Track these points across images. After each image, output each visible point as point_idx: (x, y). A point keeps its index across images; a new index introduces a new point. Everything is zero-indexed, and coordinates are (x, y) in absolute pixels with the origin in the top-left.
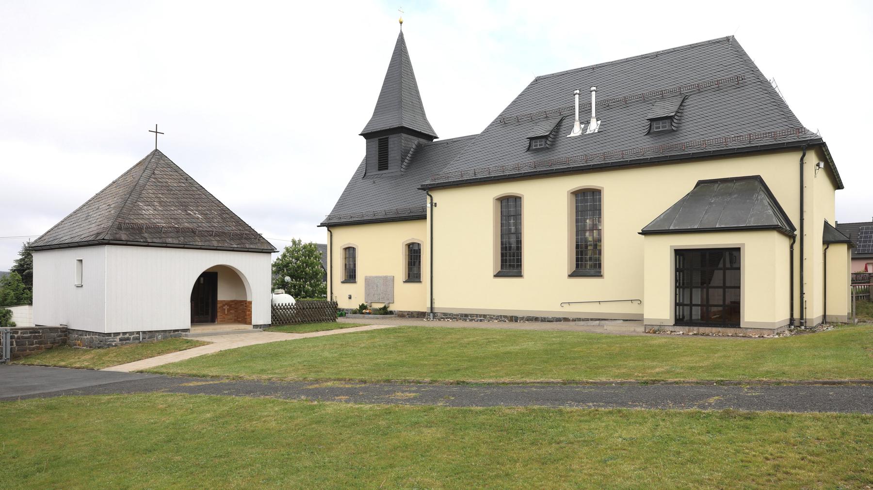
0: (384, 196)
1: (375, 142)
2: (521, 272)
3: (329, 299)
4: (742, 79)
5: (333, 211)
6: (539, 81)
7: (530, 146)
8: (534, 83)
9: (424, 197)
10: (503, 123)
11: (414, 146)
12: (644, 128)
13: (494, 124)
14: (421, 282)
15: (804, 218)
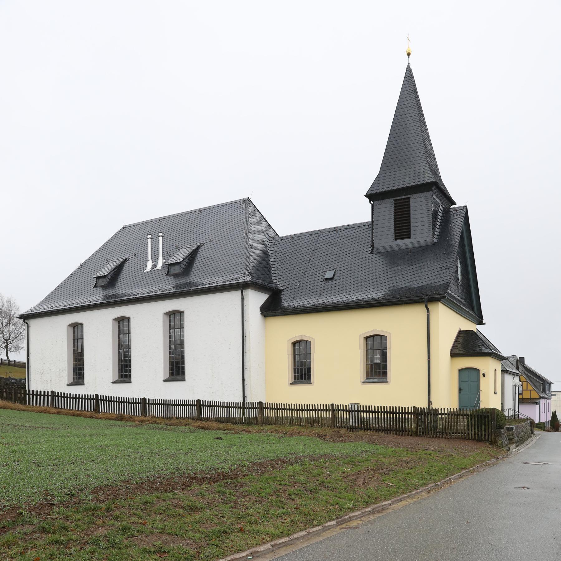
1: (388, 206)
2: (184, 378)
14: (387, 382)
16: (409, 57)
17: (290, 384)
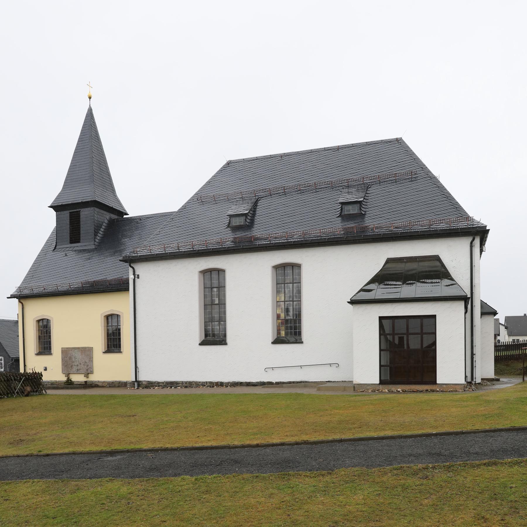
0: (78, 269)
2: (301, 339)
3: (22, 371)
4: (415, 174)
5: (23, 283)
6: (231, 165)
7: (229, 223)
8: (226, 166)
9: (127, 269)
10: (200, 201)
11: (106, 221)
12: (335, 211)
13: (190, 201)
14: (121, 352)
15: (474, 292)
16: (90, 100)
17: (103, 352)
